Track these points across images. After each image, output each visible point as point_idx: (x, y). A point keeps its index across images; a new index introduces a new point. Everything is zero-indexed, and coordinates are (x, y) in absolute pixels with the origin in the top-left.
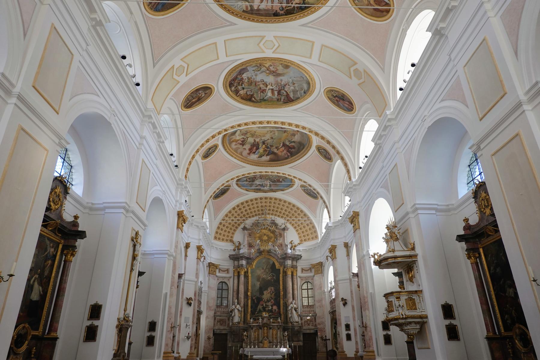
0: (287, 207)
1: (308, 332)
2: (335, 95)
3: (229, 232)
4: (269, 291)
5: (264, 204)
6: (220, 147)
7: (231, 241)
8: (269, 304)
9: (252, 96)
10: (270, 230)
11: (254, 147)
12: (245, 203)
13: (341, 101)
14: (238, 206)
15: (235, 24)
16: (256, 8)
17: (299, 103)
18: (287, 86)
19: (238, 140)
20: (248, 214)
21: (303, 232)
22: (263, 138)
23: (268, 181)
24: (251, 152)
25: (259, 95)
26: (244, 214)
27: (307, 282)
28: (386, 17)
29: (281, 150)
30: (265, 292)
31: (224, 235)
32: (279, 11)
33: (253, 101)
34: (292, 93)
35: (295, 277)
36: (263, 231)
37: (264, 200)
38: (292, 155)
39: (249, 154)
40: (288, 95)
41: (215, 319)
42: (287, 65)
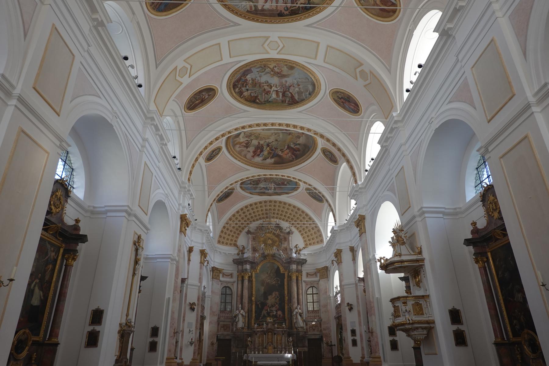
1: (313, 337)
2: (340, 97)
4: (273, 296)
5: (268, 208)
6: (224, 149)
7: (235, 245)
9: (256, 97)
10: (274, 234)
11: (259, 150)
13: (347, 103)
14: (242, 209)
18: (292, 87)
19: (242, 143)
20: (252, 217)
21: (308, 236)
22: (267, 141)
25: (264, 97)
26: (248, 217)
27: (312, 287)
28: (393, 18)
29: (286, 152)
30: (269, 297)
32: (283, 11)
33: (257, 103)
34: (297, 95)
38: (297, 157)
39: (253, 157)
40: (292, 97)
41: (218, 324)
42: (292, 66)
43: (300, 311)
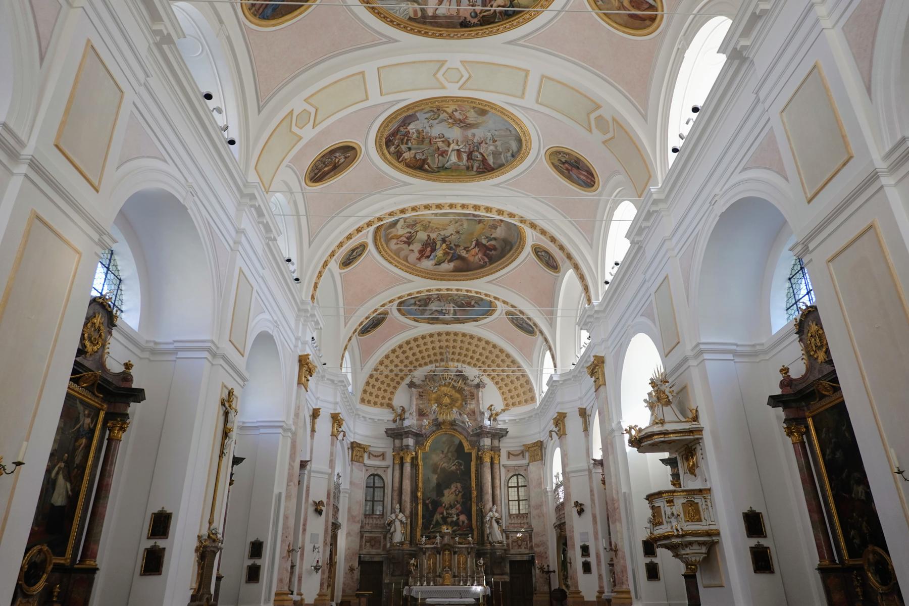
0: (484, 348)
1: (519, 558)
2: (563, 160)
3: (385, 391)
4: (453, 490)
5: (444, 344)
6: (371, 247)
7: (390, 406)
8: (453, 511)
9: (424, 161)
10: (454, 387)
11: (428, 248)
12: (412, 342)
13: (575, 170)
14: (400, 347)
15: (396, 41)
16: (430, 14)
17: (503, 174)
18: (483, 145)
19: (401, 236)
20: (417, 360)
21: (510, 391)
22: (442, 233)
23: (452, 305)
24: (422, 256)
25: (437, 160)
26: (410, 359)
27: (517, 475)
28: (650, 29)
29: (473, 252)
30: (446, 492)
31: (377, 396)
32: (469, 18)
33: (426, 171)
34: (491, 157)
35: (496, 466)
36: (443, 389)
37: (444, 337)
38: (492, 260)
39: (419, 259)
40: (484, 160)
41: (362, 537)
42: (483, 109)
43: (497, 515)
